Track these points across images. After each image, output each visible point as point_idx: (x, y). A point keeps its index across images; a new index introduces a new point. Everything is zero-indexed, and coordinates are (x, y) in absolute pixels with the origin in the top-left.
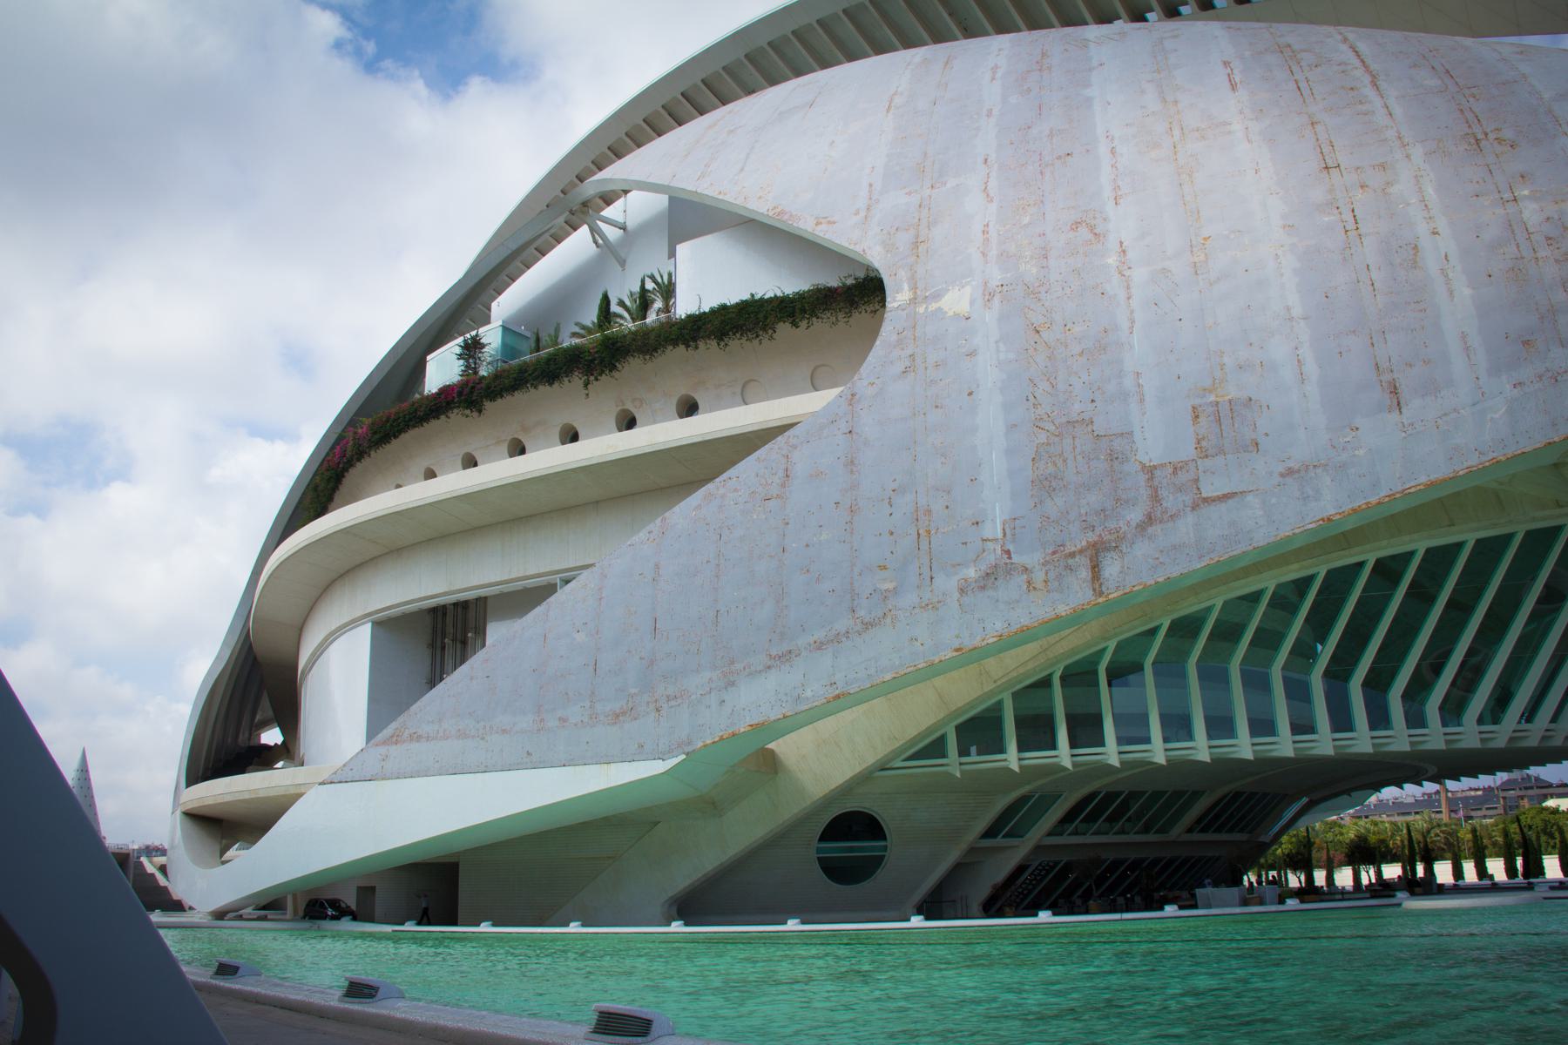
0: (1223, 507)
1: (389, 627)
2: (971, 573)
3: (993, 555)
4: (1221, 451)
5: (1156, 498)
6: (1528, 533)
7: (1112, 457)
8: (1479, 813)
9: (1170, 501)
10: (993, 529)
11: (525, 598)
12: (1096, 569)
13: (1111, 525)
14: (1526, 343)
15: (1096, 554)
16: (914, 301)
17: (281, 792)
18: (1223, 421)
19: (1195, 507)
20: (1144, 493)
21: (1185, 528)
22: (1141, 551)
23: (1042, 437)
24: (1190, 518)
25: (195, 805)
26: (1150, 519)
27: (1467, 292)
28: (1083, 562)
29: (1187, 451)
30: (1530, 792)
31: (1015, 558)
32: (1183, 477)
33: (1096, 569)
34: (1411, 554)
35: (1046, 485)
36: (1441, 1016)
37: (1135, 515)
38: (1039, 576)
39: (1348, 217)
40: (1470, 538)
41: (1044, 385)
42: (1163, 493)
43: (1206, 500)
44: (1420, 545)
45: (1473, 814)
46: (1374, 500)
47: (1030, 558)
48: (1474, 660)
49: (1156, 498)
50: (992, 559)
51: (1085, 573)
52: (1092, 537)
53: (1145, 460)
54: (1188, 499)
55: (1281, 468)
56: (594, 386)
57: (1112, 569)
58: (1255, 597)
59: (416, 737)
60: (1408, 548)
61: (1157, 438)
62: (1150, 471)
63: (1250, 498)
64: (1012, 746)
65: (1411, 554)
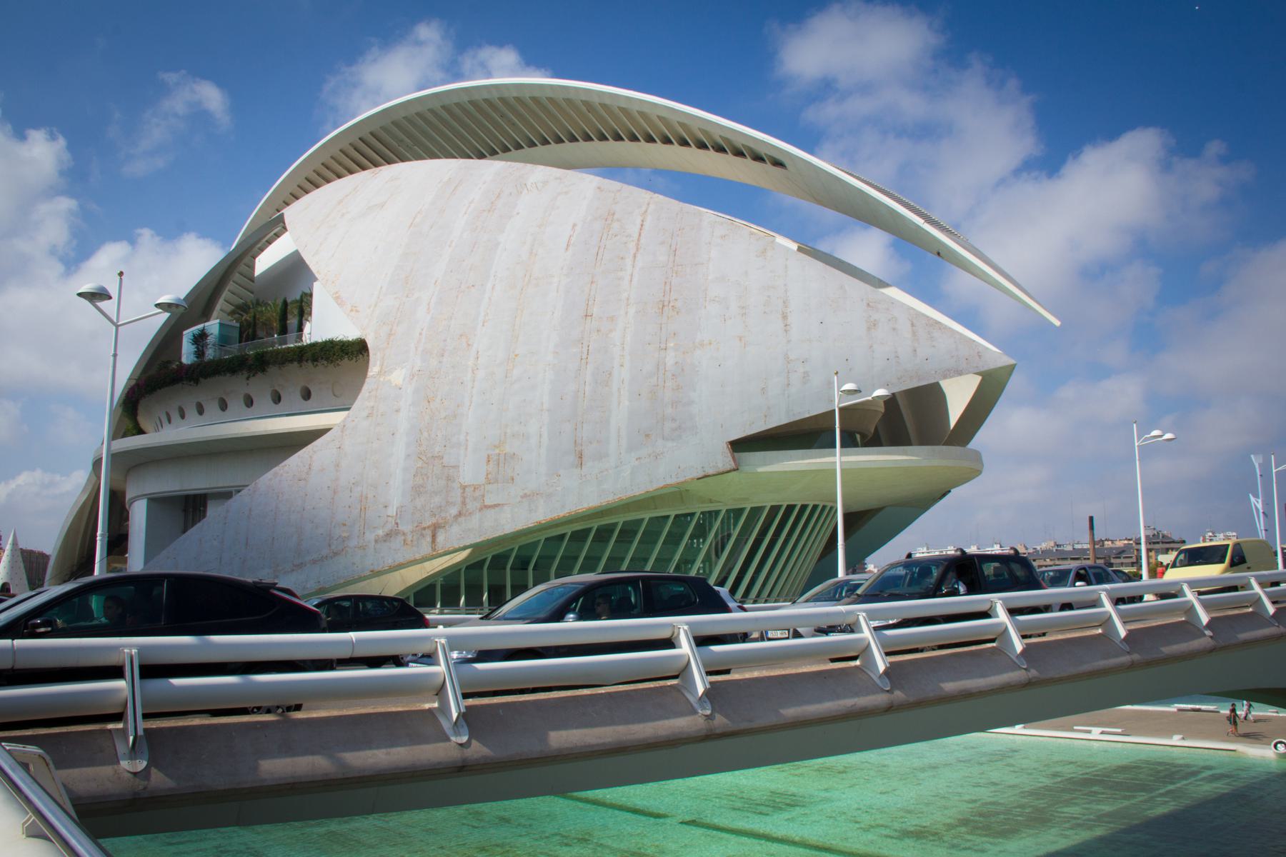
0: (493, 511)
1: (158, 503)
4: (496, 481)
5: (464, 503)
7: (449, 479)
8: (1118, 561)
9: (471, 505)
10: (392, 511)
11: (226, 495)
12: (434, 537)
13: (443, 515)
14: (647, 436)
15: (435, 528)
16: (380, 373)
18: (500, 463)
19: (481, 509)
20: (459, 500)
22: (455, 529)
23: (420, 464)
24: (478, 516)
26: (460, 514)
27: (627, 403)
28: (428, 533)
29: (482, 480)
30: (1157, 546)
31: (400, 528)
32: (478, 493)
33: (434, 537)
35: (418, 490)
38: (409, 538)
39: (585, 350)
40: (673, 513)
41: (426, 434)
44: (647, 516)
45: (1113, 561)
49: (464, 503)
51: (429, 539)
52: (434, 520)
53: (462, 481)
54: (478, 505)
56: (252, 379)
57: (441, 538)
58: (562, 537)
61: (470, 471)
62: (464, 488)
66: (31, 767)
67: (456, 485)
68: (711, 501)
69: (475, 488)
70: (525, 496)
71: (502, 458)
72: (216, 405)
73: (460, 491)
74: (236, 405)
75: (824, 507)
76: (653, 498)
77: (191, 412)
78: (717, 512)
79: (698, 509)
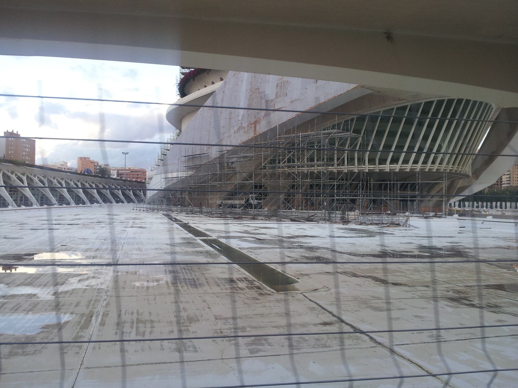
2: (236, 128)
15: (256, 123)
28: (253, 126)
29: (274, 97)
47: (245, 125)
50: (239, 125)
51: (253, 129)
57: (258, 128)
68: (400, 100)
70: (292, 102)
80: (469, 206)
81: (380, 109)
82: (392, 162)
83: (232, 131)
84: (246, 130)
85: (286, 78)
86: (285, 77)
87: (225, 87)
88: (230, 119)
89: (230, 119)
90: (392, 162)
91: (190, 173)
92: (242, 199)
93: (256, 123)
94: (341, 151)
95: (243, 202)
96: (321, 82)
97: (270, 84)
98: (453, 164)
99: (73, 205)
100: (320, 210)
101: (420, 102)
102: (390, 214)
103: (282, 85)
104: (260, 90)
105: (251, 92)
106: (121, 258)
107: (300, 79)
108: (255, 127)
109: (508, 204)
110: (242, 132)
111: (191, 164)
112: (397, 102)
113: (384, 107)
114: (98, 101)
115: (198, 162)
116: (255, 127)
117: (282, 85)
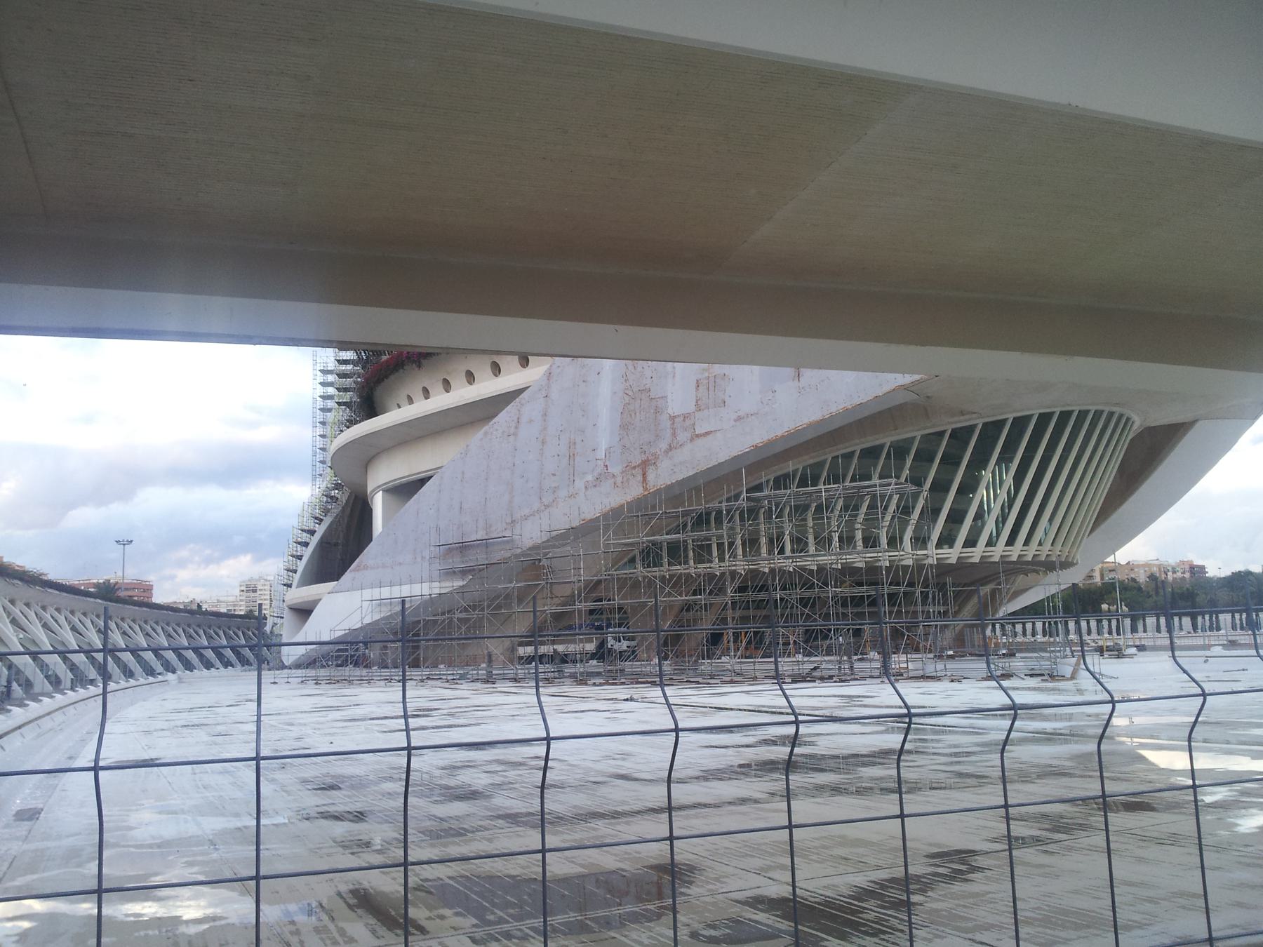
2: (590, 477)
3: (600, 469)
5: (674, 435)
6: (985, 425)
9: (683, 436)
10: (601, 454)
15: (645, 465)
17: (310, 599)
20: (669, 432)
21: (683, 454)
25: (295, 602)
26: (670, 448)
28: (638, 471)
29: (692, 408)
32: (688, 423)
34: (975, 426)
35: (625, 427)
36: (459, 767)
37: (663, 445)
42: (678, 432)
43: (697, 436)
46: (779, 434)
47: (616, 469)
48: (53, 679)
49: (674, 435)
50: (599, 470)
51: (640, 478)
52: (644, 457)
53: (670, 411)
54: (688, 435)
55: (734, 416)
57: (651, 476)
59: (366, 568)
60: (823, 458)
62: (673, 418)
63: (718, 434)
64: (691, 562)
65: (975, 426)
66: (635, 697)
67: (664, 417)
68: (962, 413)
69: (685, 417)
70: (739, 419)
71: (712, 379)
72: (440, 387)
73: (669, 423)
74: (418, 394)
75: (1121, 416)
76: (901, 408)
77: (418, 394)
78: (971, 429)
79: (949, 425)
80: (1024, 634)
81: (915, 433)
82: (939, 545)
83: (580, 484)
84: (619, 479)
85: (718, 369)
86: (717, 366)
87: (549, 386)
88: (572, 457)
89: (572, 457)
90: (939, 545)
91: (459, 583)
92: (590, 641)
93: (645, 465)
94: (872, 521)
95: (590, 647)
96: (810, 375)
97: (677, 383)
98: (1026, 543)
99: (142, 681)
100: (789, 656)
101: (1070, 408)
102: (952, 657)
103: (712, 384)
104: (652, 395)
105: (627, 398)
106: (557, 803)
107: (756, 368)
108: (644, 475)
109: (1151, 621)
110: (607, 486)
111: (457, 562)
112: (956, 419)
113: (925, 428)
114: (169, 427)
115: (477, 558)
116: (644, 475)
117: (712, 384)
